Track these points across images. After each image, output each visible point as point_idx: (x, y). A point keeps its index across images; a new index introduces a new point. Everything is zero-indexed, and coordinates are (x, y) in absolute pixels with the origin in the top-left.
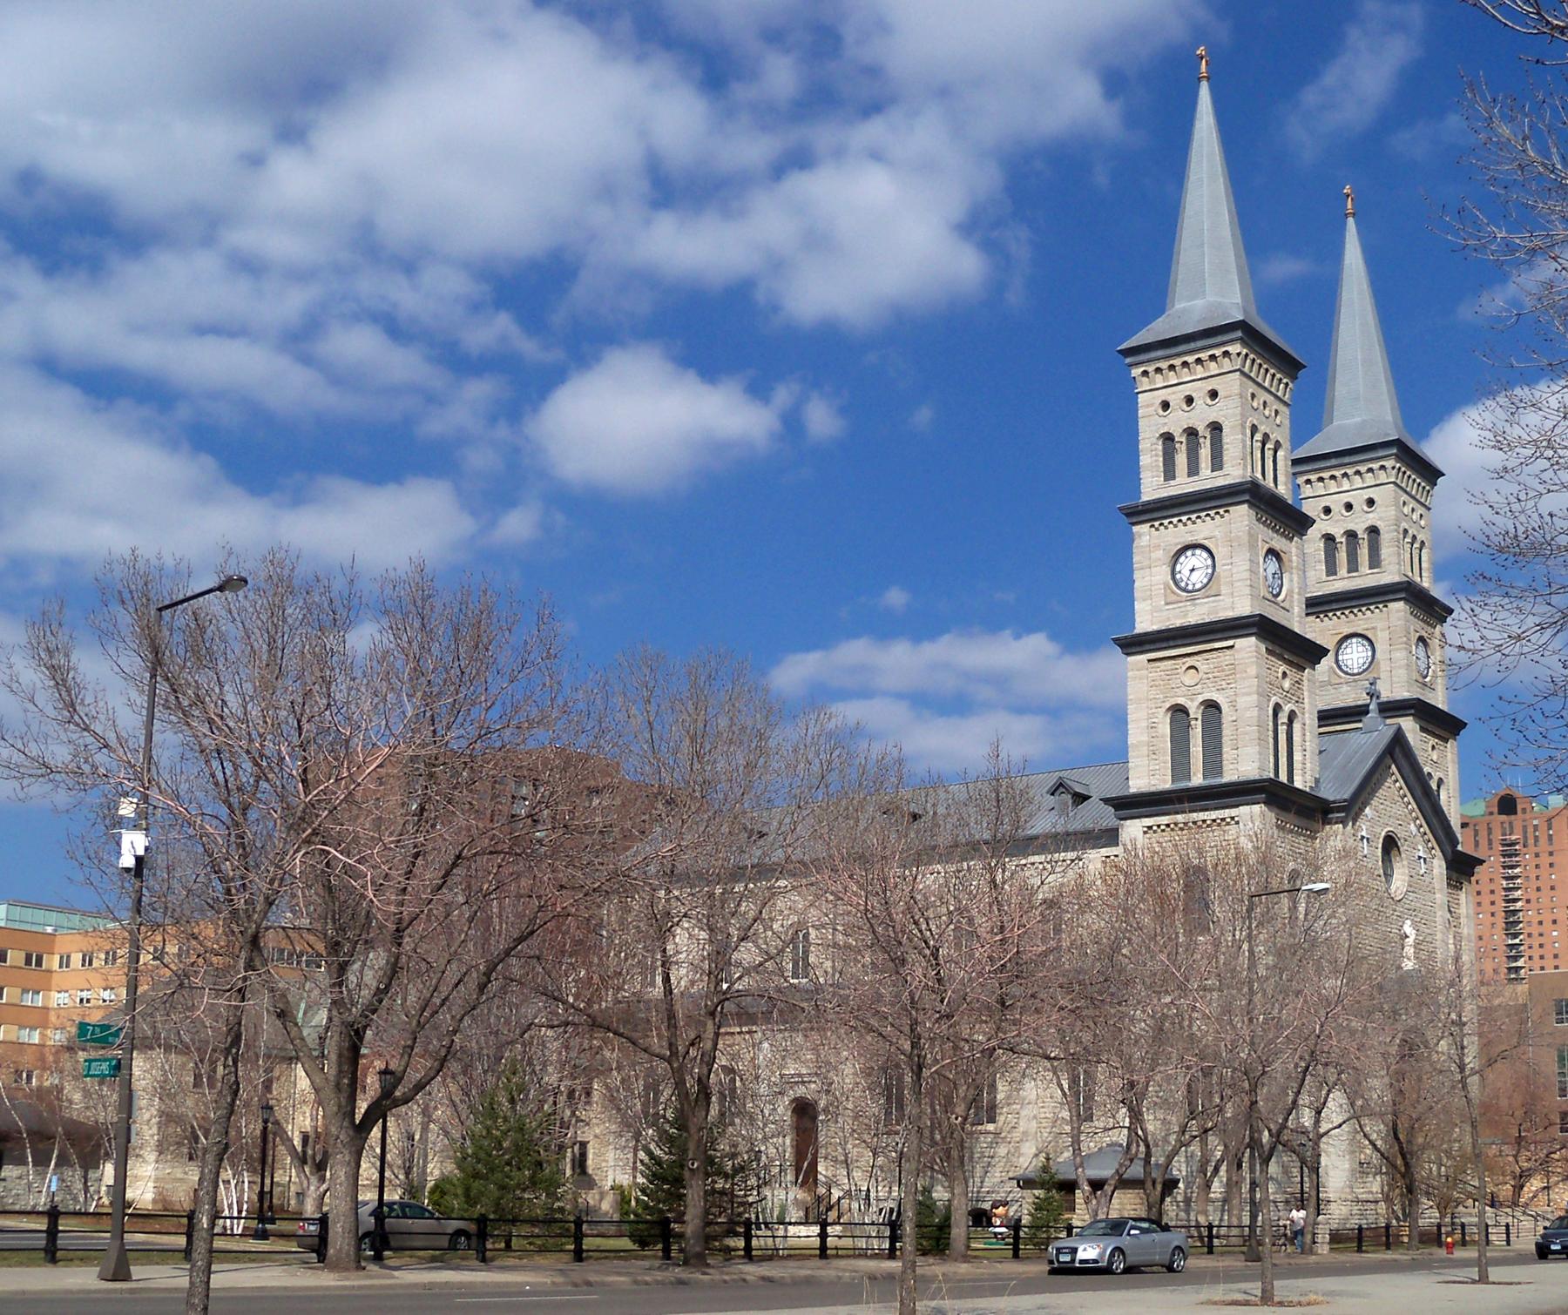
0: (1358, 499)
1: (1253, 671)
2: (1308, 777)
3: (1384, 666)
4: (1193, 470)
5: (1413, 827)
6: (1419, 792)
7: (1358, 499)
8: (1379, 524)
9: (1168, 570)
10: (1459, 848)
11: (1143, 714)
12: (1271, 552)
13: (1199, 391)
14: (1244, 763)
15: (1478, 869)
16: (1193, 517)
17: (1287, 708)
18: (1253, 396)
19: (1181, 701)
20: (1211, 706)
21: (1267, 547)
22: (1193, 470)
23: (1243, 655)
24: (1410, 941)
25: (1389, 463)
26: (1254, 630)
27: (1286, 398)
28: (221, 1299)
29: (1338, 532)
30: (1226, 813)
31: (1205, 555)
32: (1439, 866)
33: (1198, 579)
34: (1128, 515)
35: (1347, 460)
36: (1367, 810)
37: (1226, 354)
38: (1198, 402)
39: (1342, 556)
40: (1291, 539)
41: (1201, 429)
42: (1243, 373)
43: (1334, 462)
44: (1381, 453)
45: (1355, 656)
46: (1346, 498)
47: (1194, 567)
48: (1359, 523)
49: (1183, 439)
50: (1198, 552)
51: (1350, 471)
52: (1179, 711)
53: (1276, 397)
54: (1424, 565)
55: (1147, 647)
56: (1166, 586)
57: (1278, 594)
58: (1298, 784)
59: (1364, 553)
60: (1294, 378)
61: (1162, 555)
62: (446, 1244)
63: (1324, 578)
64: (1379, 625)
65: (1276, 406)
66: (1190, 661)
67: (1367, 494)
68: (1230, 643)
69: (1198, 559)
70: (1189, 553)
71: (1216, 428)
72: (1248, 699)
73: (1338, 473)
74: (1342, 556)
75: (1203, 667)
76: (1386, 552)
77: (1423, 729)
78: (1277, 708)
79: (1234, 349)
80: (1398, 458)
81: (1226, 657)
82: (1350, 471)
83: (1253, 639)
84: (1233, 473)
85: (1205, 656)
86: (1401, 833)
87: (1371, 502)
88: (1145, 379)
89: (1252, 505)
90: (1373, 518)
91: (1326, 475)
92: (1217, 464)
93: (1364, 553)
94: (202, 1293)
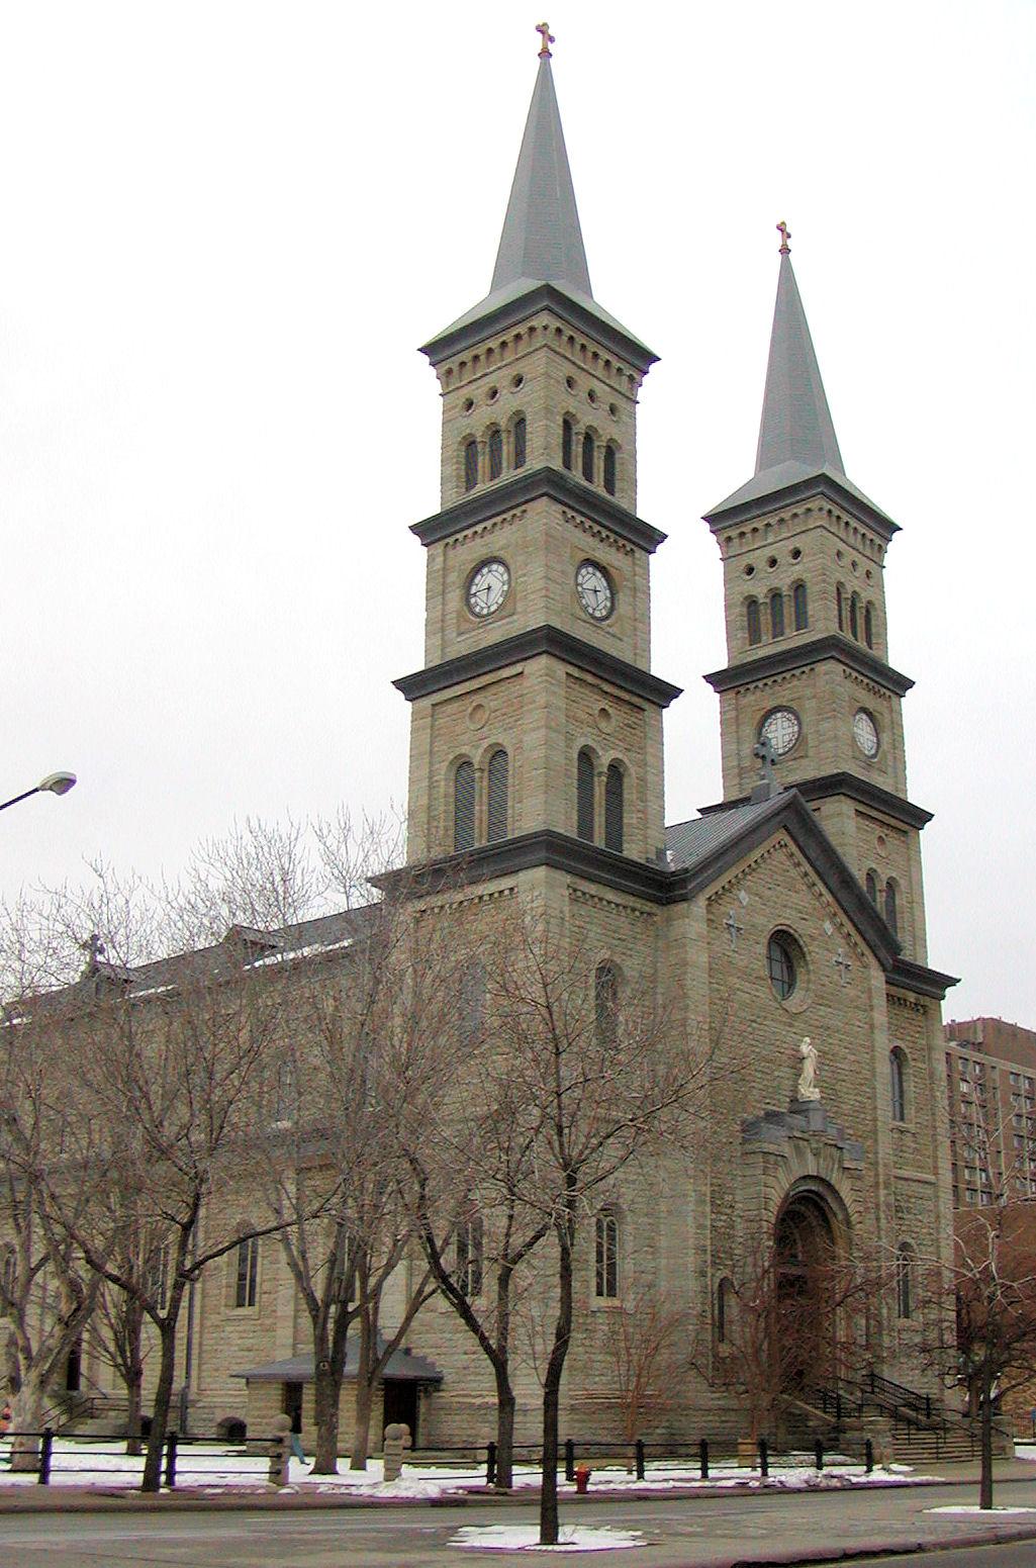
0: (781, 551)
5: (828, 926)
6: (833, 881)
7: (781, 551)
8: (806, 576)
13: (501, 378)
17: (604, 759)
19: (464, 750)
20: (498, 753)
24: (809, 1068)
30: (506, 883)
31: (501, 569)
39: (765, 618)
41: (785, 591)
46: (768, 552)
48: (783, 579)
50: (494, 567)
59: (789, 610)
66: (478, 699)
67: (791, 545)
68: (518, 668)
69: (493, 580)
70: (485, 571)
72: (534, 735)
74: (765, 618)
75: (483, 701)
76: (813, 607)
78: (586, 756)
79: (539, 321)
81: (514, 688)
82: (773, 521)
85: (493, 690)
93: (789, 610)
94: (157, 1494)
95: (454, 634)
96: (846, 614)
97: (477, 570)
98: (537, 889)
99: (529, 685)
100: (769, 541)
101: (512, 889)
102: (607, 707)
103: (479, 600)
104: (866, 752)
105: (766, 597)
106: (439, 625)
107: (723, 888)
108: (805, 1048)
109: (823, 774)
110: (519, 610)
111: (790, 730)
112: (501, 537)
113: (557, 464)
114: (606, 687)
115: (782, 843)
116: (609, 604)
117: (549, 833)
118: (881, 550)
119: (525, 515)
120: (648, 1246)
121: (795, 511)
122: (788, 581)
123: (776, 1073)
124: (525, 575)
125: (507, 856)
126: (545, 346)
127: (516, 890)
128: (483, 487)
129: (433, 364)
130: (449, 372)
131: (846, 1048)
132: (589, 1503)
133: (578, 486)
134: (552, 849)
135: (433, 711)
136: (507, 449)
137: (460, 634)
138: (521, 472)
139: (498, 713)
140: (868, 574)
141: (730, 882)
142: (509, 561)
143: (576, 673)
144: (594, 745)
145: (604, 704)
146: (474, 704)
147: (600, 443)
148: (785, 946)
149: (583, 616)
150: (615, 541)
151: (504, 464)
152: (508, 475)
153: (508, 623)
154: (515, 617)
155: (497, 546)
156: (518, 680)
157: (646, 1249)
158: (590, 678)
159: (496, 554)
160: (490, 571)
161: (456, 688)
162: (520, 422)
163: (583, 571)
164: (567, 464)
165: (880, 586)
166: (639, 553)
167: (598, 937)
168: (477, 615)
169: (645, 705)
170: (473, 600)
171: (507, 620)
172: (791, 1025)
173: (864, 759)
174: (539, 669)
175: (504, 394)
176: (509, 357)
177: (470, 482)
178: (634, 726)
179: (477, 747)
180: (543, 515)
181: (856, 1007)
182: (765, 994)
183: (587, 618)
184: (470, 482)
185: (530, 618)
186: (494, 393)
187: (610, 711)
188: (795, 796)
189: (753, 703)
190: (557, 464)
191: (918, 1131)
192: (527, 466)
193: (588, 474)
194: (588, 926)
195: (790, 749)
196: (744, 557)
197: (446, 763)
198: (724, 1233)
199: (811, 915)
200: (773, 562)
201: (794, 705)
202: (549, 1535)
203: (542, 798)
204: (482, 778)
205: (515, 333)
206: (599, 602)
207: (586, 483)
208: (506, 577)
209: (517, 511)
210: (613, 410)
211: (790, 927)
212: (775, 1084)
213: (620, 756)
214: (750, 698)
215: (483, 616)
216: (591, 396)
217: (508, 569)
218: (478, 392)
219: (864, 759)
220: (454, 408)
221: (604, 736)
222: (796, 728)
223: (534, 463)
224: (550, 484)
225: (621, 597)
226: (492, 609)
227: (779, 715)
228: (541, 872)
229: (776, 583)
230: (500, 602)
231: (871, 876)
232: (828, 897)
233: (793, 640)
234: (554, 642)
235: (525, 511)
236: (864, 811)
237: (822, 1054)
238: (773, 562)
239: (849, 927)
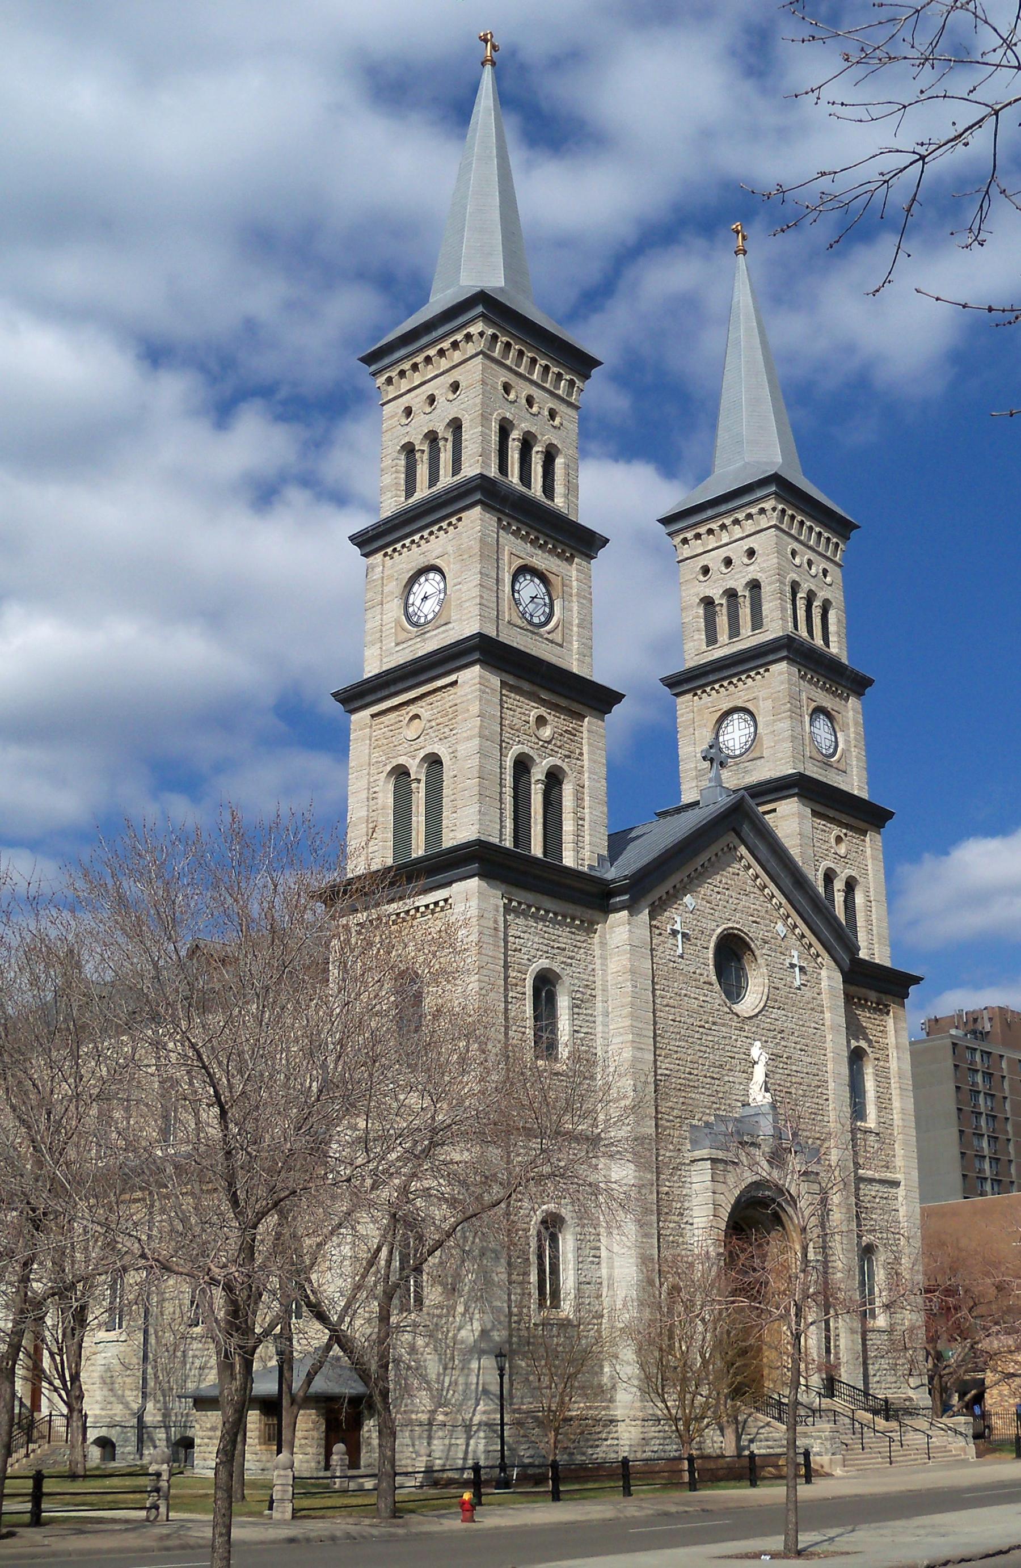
1: (475, 708)
2: (586, 854)
3: (767, 742)
4: (734, 631)
5: (780, 927)
9: (401, 603)
10: (863, 954)
11: (363, 783)
12: (819, 711)
13: (439, 387)
14: (461, 828)
15: (912, 989)
16: (426, 533)
18: (794, 553)
19: (401, 760)
21: (813, 705)
22: (734, 631)
23: (467, 689)
25: (768, 505)
26: (476, 656)
27: (837, 559)
28: (803, 1502)
29: (716, 592)
31: (438, 577)
32: (830, 979)
33: (429, 608)
34: (670, 686)
35: (723, 508)
36: (688, 899)
37: (762, 511)
38: (440, 400)
40: (847, 700)
41: (440, 429)
42: (487, 357)
43: (710, 513)
44: (759, 494)
45: (737, 735)
46: (723, 553)
47: (736, 735)
48: (738, 581)
49: (724, 601)
50: (431, 575)
51: (728, 521)
52: (401, 773)
53: (824, 557)
54: (832, 628)
55: (369, 699)
56: (398, 622)
57: (833, 755)
58: (568, 860)
60: (846, 538)
61: (394, 587)
62: (27, 1518)
63: (704, 647)
64: (761, 695)
65: (824, 564)
66: (413, 709)
67: (746, 544)
68: (452, 678)
69: (430, 585)
70: (422, 579)
71: (755, 586)
73: (714, 526)
75: (420, 711)
76: (770, 607)
77: (815, 813)
78: (522, 766)
80: (778, 496)
83: (477, 668)
84: (774, 628)
85: (429, 699)
86: (754, 933)
87: (751, 553)
88: (391, 388)
89: (487, 507)
90: (753, 572)
91: (702, 530)
92: (757, 622)
96: (801, 614)
97: (413, 579)
98: (469, 897)
99: (462, 693)
100: (723, 542)
101: (446, 900)
102: (545, 714)
104: (824, 751)
105: (721, 597)
106: (378, 635)
107: (667, 893)
108: (756, 1051)
109: (779, 774)
111: (726, 737)
112: (436, 545)
113: (493, 472)
115: (731, 845)
116: (547, 610)
117: (479, 842)
120: (594, 1256)
121: (749, 511)
122: (744, 581)
123: (726, 1078)
125: (443, 866)
126: (481, 352)
127: (450, 901)
128: (422, 492)
131: (801, 1050)
132: (586, 1479)
133: (512, 491)
134: (481, 859)
137: (397, 644)
141: (675, 887)
142: (446, 570)
144: (531, 753)
145: (542, 711)
146: (411, 714)
148: (732, 953)
149: (519, 622)
152: (446, 480)
154: (450, 626)
155: (435, 554)
156: (452, 690)
157: (591, 1259)
159: (433, 562)
160: (427, 580)
162: (456, 425)
164: (503, 468)
167: (535, 946)
172: (741, 1029)
173: (820, 758)
174: (472, 677)
177: (410, 488)
178: (574, 732)
179: (414, 757)
180: (475, 521)
181: (812, 1009)
182: (716, 996)
183: (525, 624)
184: (410, 488)
185: (465, 625)
188: (743, 798)
189: (710, 705)
190: (493, 472)
191: (882, 1130)
192: (462, 474)
193: (525, 477)
194: (526, 936)
195: (747, 750)
197: (385, 774)
198: (673, 1242)
199: (763, 918)
200: (728, 562)
201: (750, 706)
202: (680, 1419)
203: (477, 806)
204: (418, 788)
205: (452, 340)
207: (524, 489)
208: (442, 585)
211: (742, 931)
212: (726, 1088)
213: (559, 763)
219: (820, 758)
221: (541, 743)
222: (752, 729)
223: (470, 469)
224: (487, 492)
226: (429, 617)
227: (736, 716)
228: (474, 882)
230: (436, 610)
231: (829, 877)
232: (780, 898)
233: (749, 639)
234: (486, 650)
236: (822, 811)
237: (774, 1057)
238: (728, 562)
239: (803, 928)
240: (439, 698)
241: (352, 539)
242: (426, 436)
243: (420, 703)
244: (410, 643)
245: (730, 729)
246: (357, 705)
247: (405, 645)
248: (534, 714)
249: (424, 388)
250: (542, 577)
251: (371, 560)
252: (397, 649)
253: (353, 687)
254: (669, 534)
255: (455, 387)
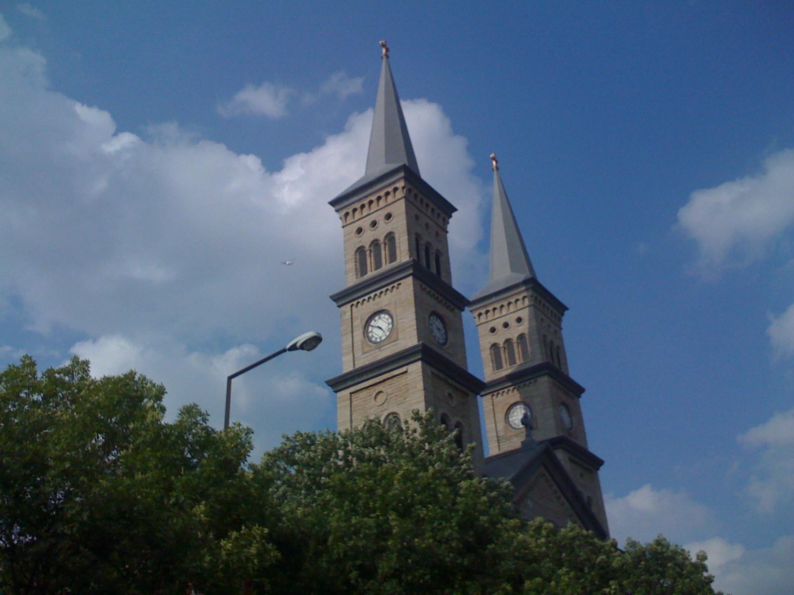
13: (379, 216)
29: (501, 341)
31: (387, 316)
43: (494, 299)
46: (503, 320)
50: (382, 316)
68: (404, 369)
69: (383, 322)
70: (377, 318)
81: (403, 380)
95: (361, 354)
97: (371, 317)
103: (374, 335)
110: (400, 338)
111: (514, 418)
112: (385, 300)
114: (450, 381)
118: (560, 320)
119: (400, 286)
124: (402, 319)
128: (371, 274)
129: (337, 211)
130: (347, 214)
135: (351, 397)
136: (384, 253)
137: (363, 354)
138: (395, 264)
139: (393, 395)
140: (556, 332)
142: (393, 312)
143: (436, 372)
147: (433, 251)
150: (446, 303)
151: (383, 261)
152: (386, 267)
153: (393, 345)
154: (398, 342)
156: (405, 376)
158: (442, 376)
159: (384, 308)
161: (365, 383)
162: (390, 237)
163: (432, 318)
165: (561, 339)
166: (456, 311)
168: (375, 343)
169: (470, 393)
170: (370, 335)
171: (393, 343)
175: (381, 223)
176: (382, 203)
177: (363, 272)
186: (374, 224)
187: (453, 394)
196: (490, 323)
206: (439, 335)
208: (390, 321)
209: (395, 284)
210: (437, 234)
214: (500, 397)
215: (378, 343)
216: (427, 225)
217: (391, 317)
218: (365, 223)
220: (350, 233)
225: (450, 334)
229: (509, 336)
235: (400, 284)
240: (395, 381)
241: (331, 297)
242: (373, 242)
243: (382, 384)
244: (372, 352)
245: (515, 414)
246: (339, 388)
247: (390, 345)
248: (447, 391)
249: (369, 217)
250: (441, 318)
251: (343, 308)
252: (364, 356)
253: (340, 377)
254: (471, 311)
255: (389, 216)
